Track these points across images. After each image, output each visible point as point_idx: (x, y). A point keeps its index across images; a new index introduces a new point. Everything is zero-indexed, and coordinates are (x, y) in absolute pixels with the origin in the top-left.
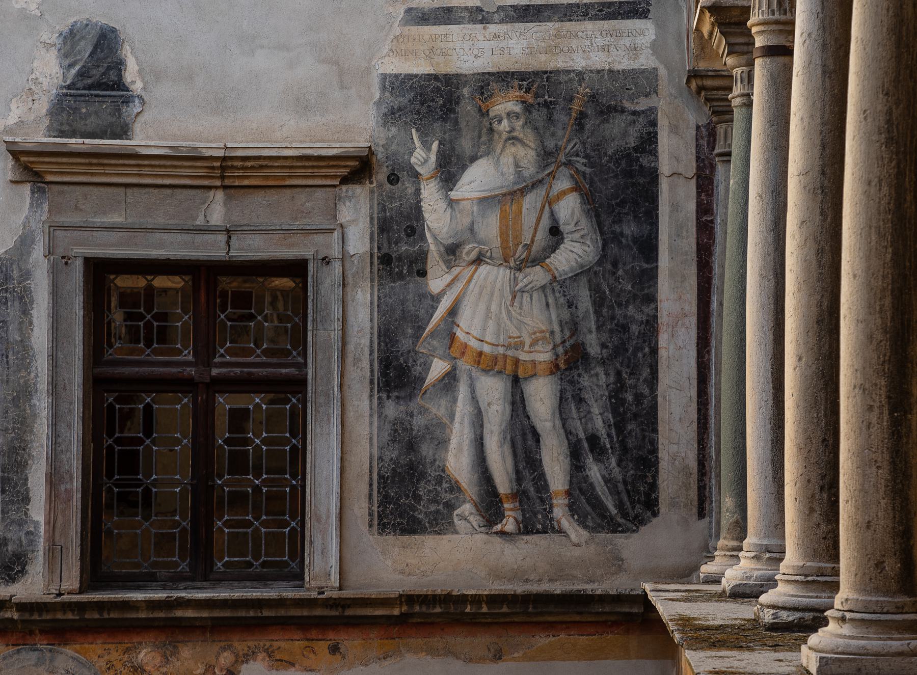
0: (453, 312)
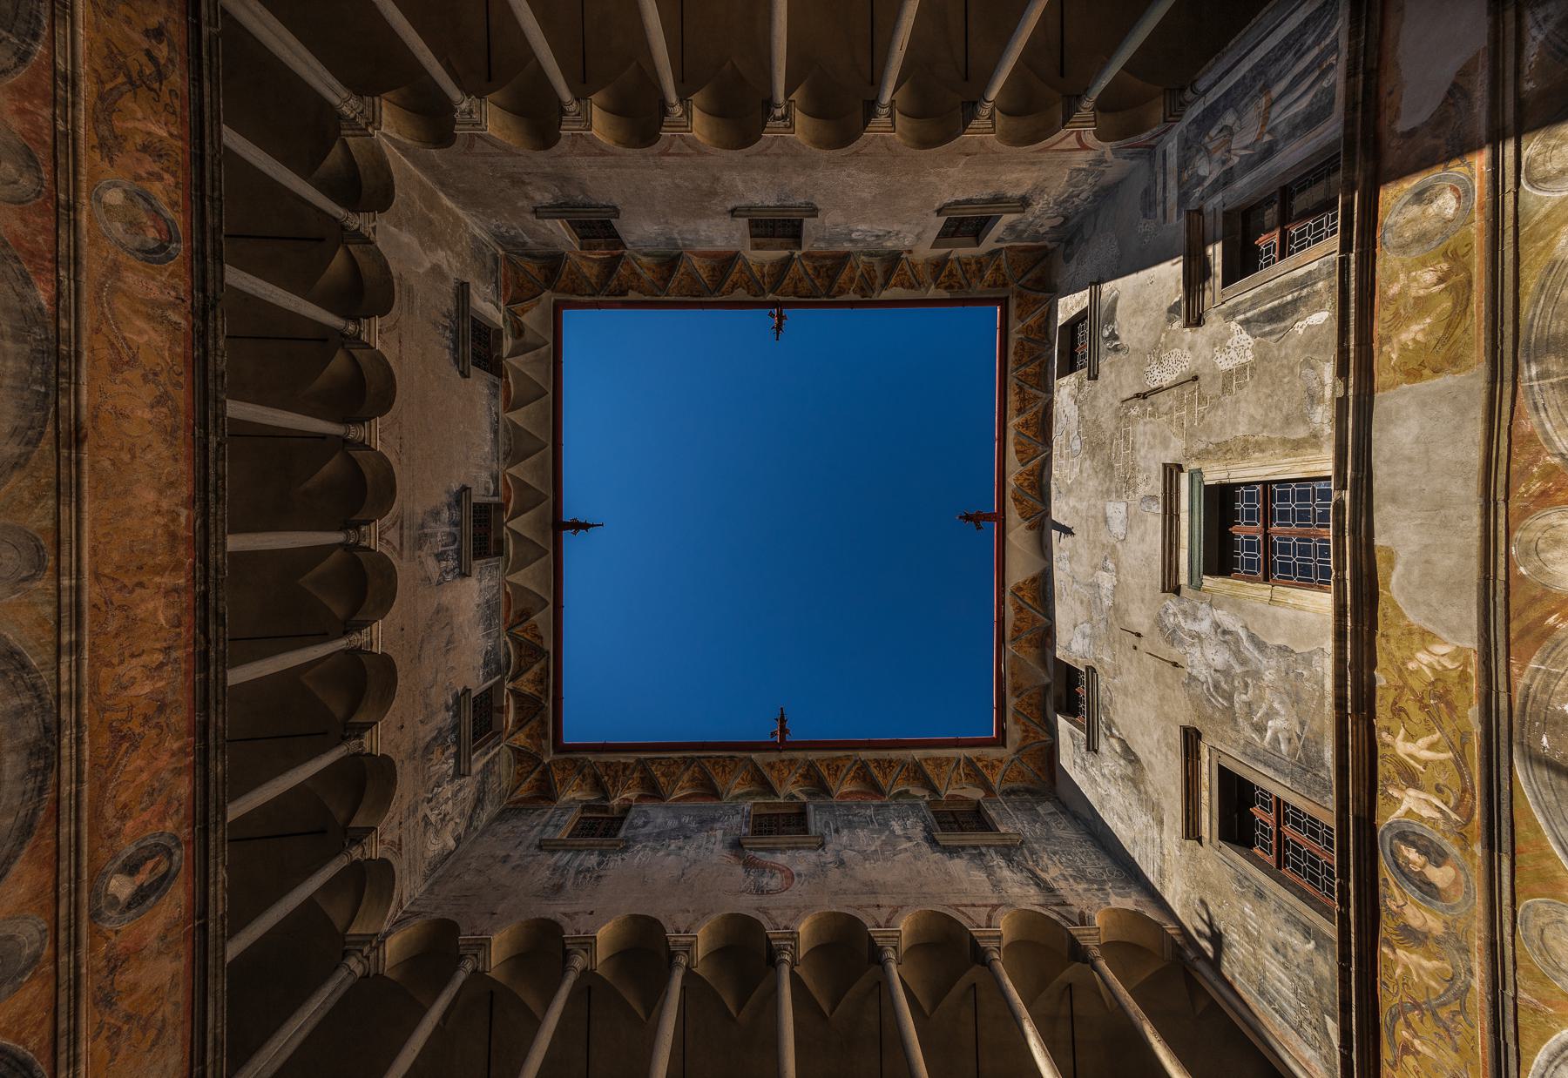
0: (1246, 148)
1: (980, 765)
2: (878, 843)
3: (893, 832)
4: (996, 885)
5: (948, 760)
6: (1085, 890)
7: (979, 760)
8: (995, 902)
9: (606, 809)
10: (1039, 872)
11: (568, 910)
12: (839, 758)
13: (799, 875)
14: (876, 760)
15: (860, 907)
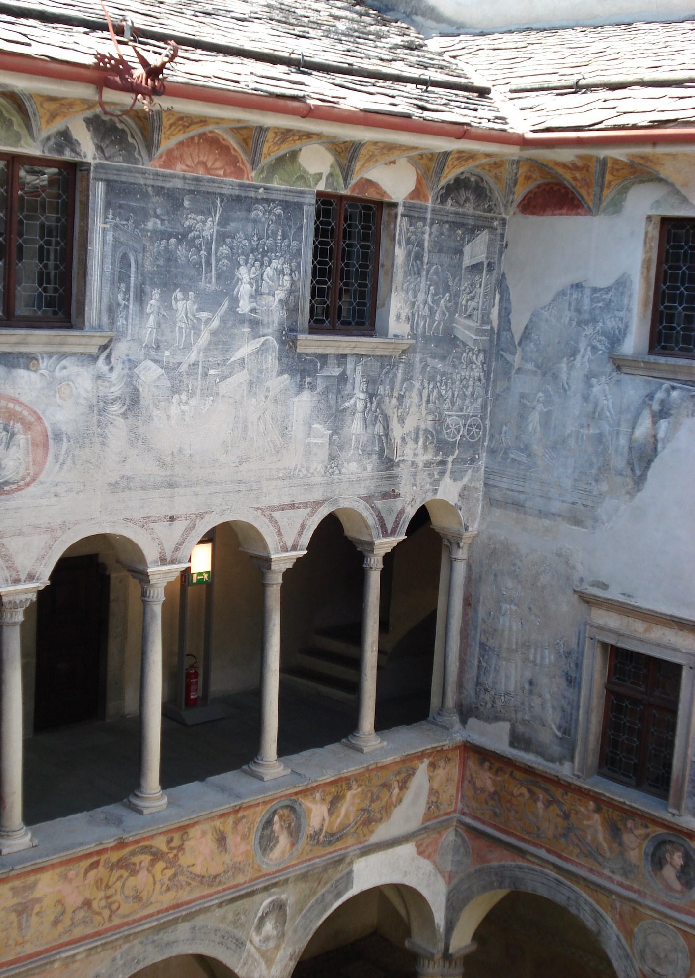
3: (235, 300)
15: (146, 523)
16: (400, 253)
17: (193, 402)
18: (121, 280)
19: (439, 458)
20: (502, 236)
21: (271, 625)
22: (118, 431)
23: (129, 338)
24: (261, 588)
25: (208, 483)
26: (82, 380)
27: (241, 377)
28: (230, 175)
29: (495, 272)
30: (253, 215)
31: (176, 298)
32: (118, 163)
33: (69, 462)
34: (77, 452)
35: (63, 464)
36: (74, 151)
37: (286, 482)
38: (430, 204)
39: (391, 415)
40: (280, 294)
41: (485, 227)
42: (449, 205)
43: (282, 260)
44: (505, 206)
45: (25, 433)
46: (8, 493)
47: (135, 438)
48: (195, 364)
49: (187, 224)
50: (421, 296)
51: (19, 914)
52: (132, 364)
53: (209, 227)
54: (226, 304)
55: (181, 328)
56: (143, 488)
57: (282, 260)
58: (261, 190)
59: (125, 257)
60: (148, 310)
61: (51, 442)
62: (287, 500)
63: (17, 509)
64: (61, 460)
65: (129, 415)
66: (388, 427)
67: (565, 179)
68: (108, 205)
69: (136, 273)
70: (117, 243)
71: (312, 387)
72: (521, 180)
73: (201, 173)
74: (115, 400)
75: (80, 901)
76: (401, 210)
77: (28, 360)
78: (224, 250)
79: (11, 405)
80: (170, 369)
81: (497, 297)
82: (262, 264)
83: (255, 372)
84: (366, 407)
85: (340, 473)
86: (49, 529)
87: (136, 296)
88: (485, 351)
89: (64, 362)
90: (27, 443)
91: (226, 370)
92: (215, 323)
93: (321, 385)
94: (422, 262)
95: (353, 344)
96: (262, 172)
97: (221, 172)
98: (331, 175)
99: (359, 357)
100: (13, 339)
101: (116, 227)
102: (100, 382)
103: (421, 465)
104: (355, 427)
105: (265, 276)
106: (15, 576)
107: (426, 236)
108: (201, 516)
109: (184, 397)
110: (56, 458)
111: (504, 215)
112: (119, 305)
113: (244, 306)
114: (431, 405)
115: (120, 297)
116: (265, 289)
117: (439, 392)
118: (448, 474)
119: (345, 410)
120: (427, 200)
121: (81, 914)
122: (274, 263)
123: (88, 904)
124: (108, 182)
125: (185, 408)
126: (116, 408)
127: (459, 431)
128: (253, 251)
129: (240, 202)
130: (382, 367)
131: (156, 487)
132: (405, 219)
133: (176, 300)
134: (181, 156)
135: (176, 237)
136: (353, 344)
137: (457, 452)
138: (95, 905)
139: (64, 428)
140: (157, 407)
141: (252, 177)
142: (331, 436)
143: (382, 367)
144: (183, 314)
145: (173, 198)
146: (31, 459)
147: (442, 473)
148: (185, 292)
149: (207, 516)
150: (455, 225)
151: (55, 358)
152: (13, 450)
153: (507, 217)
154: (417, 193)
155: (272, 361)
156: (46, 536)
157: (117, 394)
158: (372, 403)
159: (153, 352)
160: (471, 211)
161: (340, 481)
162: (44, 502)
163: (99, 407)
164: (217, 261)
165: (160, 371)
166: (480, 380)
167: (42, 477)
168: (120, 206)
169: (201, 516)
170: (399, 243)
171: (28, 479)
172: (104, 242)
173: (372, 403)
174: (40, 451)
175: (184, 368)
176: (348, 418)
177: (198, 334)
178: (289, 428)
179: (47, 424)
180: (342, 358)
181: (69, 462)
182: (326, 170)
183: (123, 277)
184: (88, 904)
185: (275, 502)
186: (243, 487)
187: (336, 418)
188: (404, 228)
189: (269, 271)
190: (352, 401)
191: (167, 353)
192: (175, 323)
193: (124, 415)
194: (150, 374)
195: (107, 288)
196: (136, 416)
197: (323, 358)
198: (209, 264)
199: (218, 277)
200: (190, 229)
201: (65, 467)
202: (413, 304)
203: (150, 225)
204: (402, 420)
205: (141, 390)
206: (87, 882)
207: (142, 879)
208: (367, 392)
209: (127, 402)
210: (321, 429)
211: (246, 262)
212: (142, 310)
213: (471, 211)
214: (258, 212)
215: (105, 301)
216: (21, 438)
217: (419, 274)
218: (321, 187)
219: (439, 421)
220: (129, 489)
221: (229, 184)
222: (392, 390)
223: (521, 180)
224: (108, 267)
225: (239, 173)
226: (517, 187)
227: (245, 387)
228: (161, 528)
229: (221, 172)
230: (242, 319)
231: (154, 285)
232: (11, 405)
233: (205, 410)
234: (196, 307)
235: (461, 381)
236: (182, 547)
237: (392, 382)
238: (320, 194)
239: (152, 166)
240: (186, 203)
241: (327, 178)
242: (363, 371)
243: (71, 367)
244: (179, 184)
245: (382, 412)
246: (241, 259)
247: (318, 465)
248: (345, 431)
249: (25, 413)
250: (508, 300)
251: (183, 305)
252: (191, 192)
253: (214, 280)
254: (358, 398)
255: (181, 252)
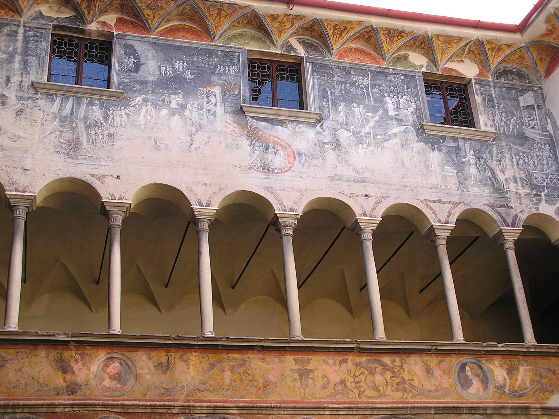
1: (487, 47)
2: (372, 123)
3: (386, 111)
4: (444, 178)
5: (460, 39)
6: (527, 195)
7: (489, 42)
8: (456, 199)
9: (83, 31)
10: (498, 172)
11: (95, 172)
12: (351, 22)
13: (300, 154)
14: (388, 30)
15: (351, 196)
16: (478, 99)
17: (370, 148)
18: (324, 97)
19: (534, 192)
20: (542, 94)
21: (444, 265)
22: (331, 156)
23: (331, 119)
24: (435, 248)
25: (386, 184)
26: (310, 134)
27: (397, 141)
28: (373, 63)
29: (543, 109)
30: (389, 78)
31: (353, 106)
32: (316, 56)
33: (307, 164)
34: (310, 161)
35: (303, 165)
36: (294, 52)
37: (434, 190)
38: (490, 79)
39: (495, 168)
40: (411, 110)
41: (529, 90)
42: (503, 80)
43: (409, 96)
44: (538, 80)
45: (283, 150)
46: (277, 173)
47: (340, 159)
48: (369, 133)
49: (354, 79)
50: (497, 117)
51: (301, 375)
52: (335, 130)
53: (367, 81)
54: (381, 111)
55: (358, 118)
56: (348, 181)
57: (409, 96)
58: (391, 70)
59: (324, 89)
60: (340, 110)
61: (297, 156)
62: (436, 199)
63: (282, 180)
64: (302, 163)
65: (336, 150)
66: (494, 174)
67: (551, 43)
68: (313, 71)
69: (331, 95)
70: (320, 85)
71: (440, 150)
72: (538, 62)
73: (358, 62)
74: (328, 143)
75: (338, 380)
76: (473, 81)
77: (282, 123)
78: (376, 90)
79: (275, 139)
80: (356, 134)
81: (549, 120)
82: (398, 97)
83: (403, 140)
84: (477, 163)
85: (468, 191)
86: (299, 191)
87: (332, 105)
88: (549, 144)
89: (300, 126)
90: (285, 155)
91: (387, 138)
92: (377, 118)
93: (444, 150)
94: (494, 103)
95: (458, 131)
96: (390, 63)
97: (369, 62)
98: (428, 65)
99: (466, 140)
100: (273, 112)
101: (318, 79)
102: (318, 135)
103: (523, 195)
104: (473, 170)
105: (400, 102)
106: (283, 208)
107: (493, 92)
108: (385, 198)
109: (365, 146)
110: (300, 162)
111: (540, 85)
112: (324, 107)
113: (392, 113)
114: (520, 166)
115: (324, 104)
116: (401, 106)
117: (524, 161)
118: (543, 201)
119: (463, 162)
120: (488, 78)
121: (340, 388)
122: (405, 97)
123: (343, 382)
124: (312, 63)
125: (367, 150)
126: (328, 146)
127: (544, 181)
128: (391, 92)
129: (382, 73)
130: (482, 146)
131: (356, 181)
132: (477, 85)
133: (354, 107)
134: (347, 56)
135: (349, 84)
136: (458, 131)
137: (546, 191)
138: (348, 384)
139: (303, 151)
140: (351, 148)
141: (385, 64)
142: (457, 173)
143: (482, 146)
144: (358, 113)
145: (346, 71)
146: (287, 161)
147: (540, 200)
148: (358, 104)
149: (387, 199)
150: (509, 89)
151: (295, 123)
152: (278, 157)
153: (542, 86)
154: (480, 74)
155: (412, 136)
156: (298, 193)
157: (329, 141)
158: (480, 161)
159: (345, 126)
160: (518, 83)
161: (469, 195)
162: (295, 179)
163: (321, 144)
164: (373, 94)
165: (350, 134)
166: (551, 158)
167: (293, 169)
168: (320, 71)
169: (385, 198)
170: (477, 94)
171: (286, 169)
172: (313, 83)
173: (480, 161)
174: (292, 159)
175: (363, 134)
176: (467, 167)
177: (368, 121)
178: (430, 166)
179: (294, 148)
180: (455, 139)
181: (307, 164)
182: (425, 64)
183: (325, 96)
184: (343, 382)
185: (429, 198)
186: (406, 188)
187: (460, 166)
188: (478, 89)
189: (402, 100)
190: (467, 159)
191: (352, 127)
192: (355, 116)
193: (334, 149)
194: (344, 135)
195: (317, 100)
196: (340, 150)
197: (444, 138)
198: (368, 95)
199: (375, 100)
200: (356, 82)
201: (305, 167)
202: (494, 120)
203: (335, 79)
204: (503, 172)
205: (341, 140)
206: (341, 369)
207: (379, 378)
208: (475, 156)
209: (334, 144)
210: (450, 171)
211: (389, 96)
212: (336, 110)
213: (518, 83)
214: (391, 77)
215: (317, 105)
216: (281, 152)
217: (494, 108)
218: (424, 70)
219: (529, 175)
220: (341, 180)
221: (374, 66)
222: (492, 157)
223: (538, 62)
224: (317, 93)
225: (378, 63)
226: (539, 66)
227: (399, 145)
228: (362, 200)
229: (369, 62)
230: (391, 118)
231: (341, 101)
232: (275, 139)
233: (378, 153)
234: (365, 111)
235: (538, 157)
236: (376, 211)
237: (491, 153)
238: (423, 73)
239: (333, 58)
240: (352, 72)
241: (426, 67)
242: (470, 146)
243: (303, 128)
244: (348, 65)
245: (488, 166)
246: (386, 95)
247: (453, 183)
248: (466, 172)
249: (282, 143)
250: (554, 118)
251: (358, 110)
252: (353, 68)
253: (372, 101)
254: (470, 157)
255: (353, 89)
